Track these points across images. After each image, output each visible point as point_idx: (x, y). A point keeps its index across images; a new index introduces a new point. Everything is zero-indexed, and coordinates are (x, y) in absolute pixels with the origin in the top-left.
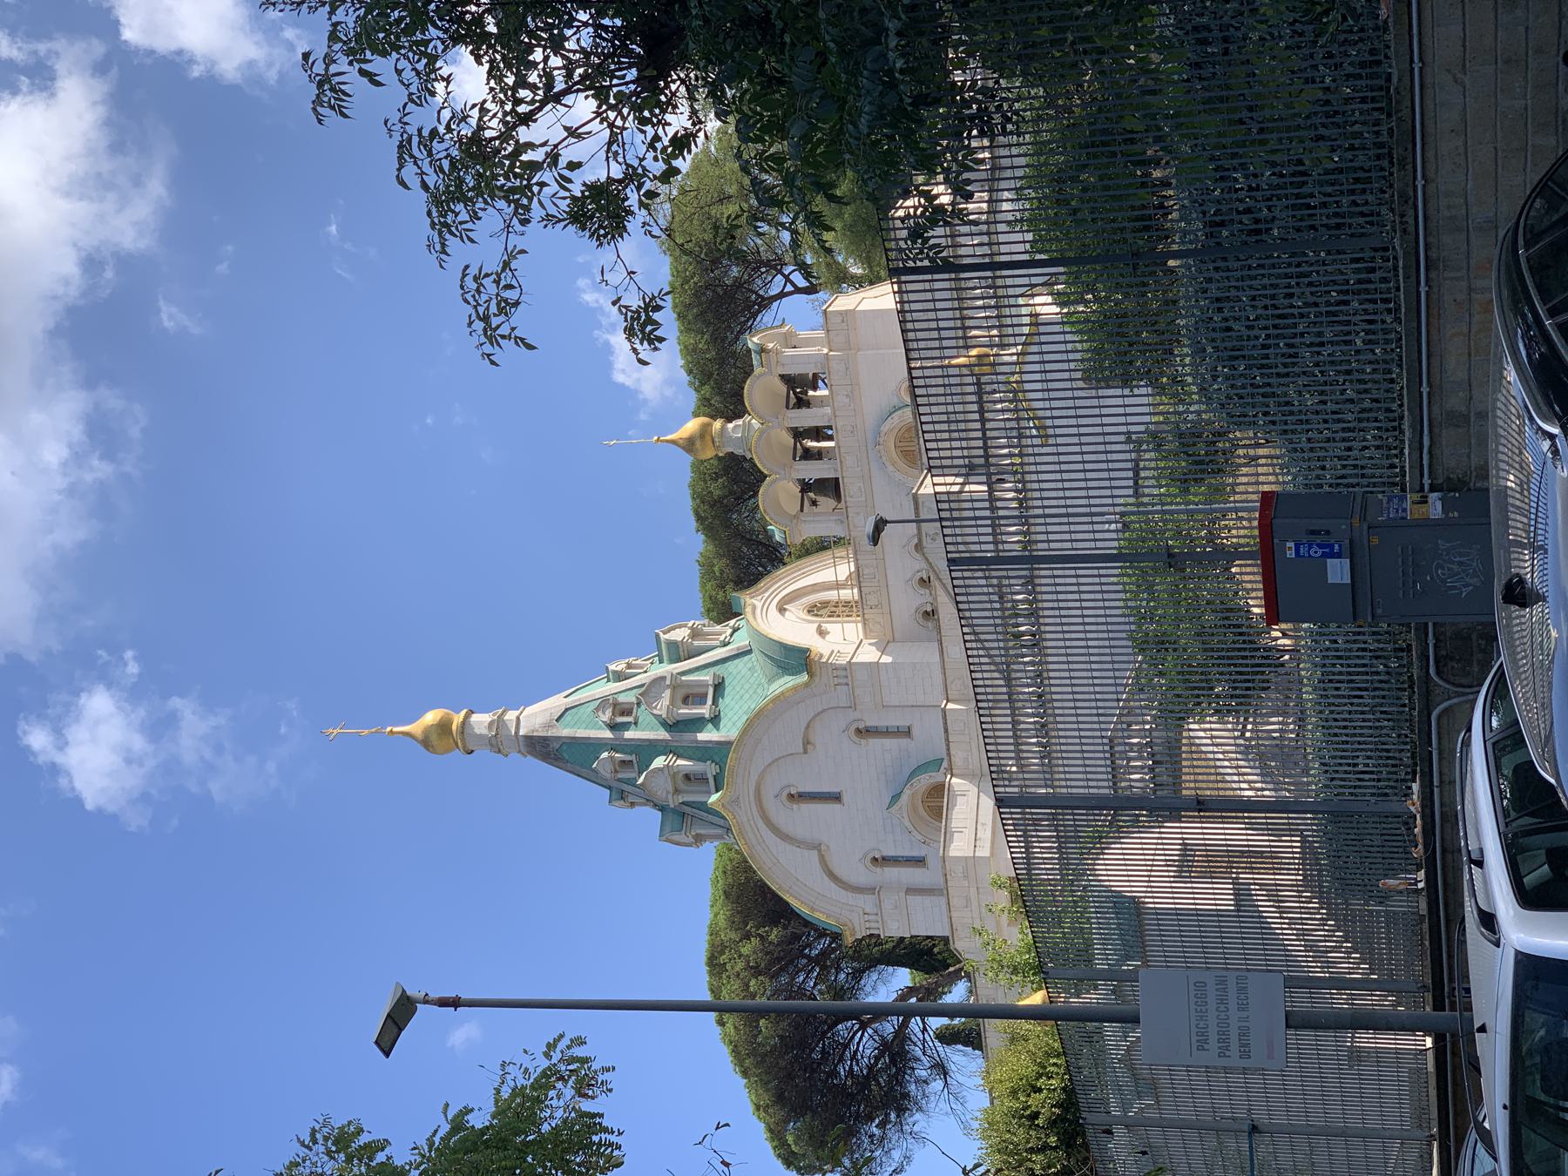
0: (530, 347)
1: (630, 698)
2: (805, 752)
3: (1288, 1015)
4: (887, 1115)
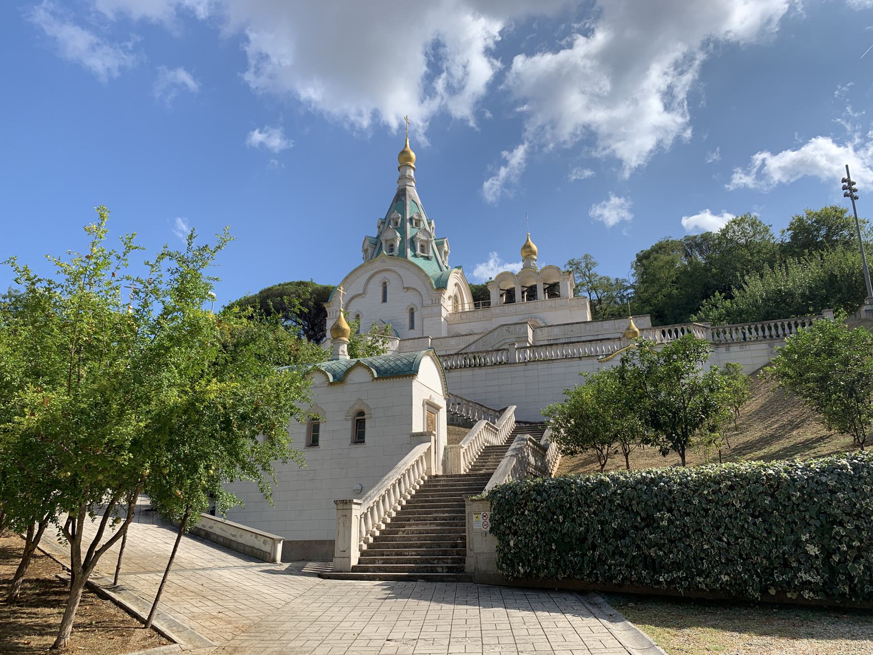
1: (422, 226)
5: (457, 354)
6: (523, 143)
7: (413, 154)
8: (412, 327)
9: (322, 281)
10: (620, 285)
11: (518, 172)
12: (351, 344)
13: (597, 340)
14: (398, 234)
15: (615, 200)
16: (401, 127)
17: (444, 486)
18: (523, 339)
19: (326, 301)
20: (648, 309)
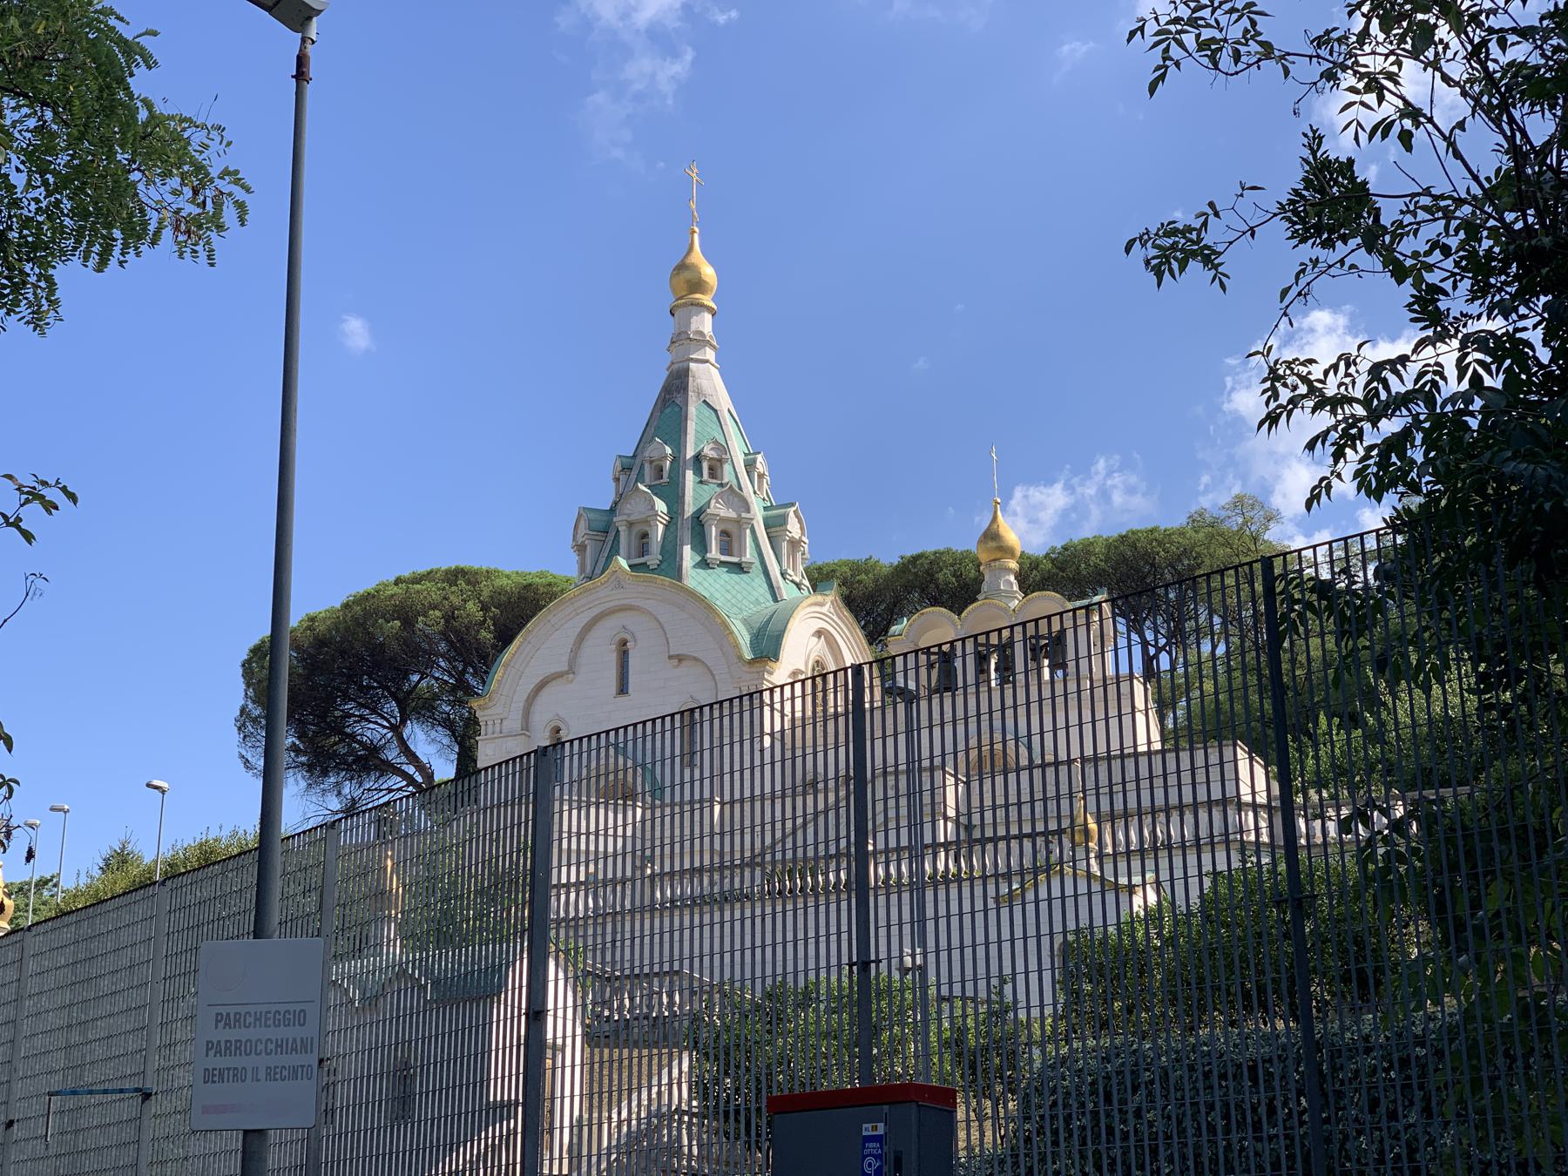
0: (1152, 89)
1: (727, 475)
2: (670, 657)
3: (261, 1133)
4: (305, 753)
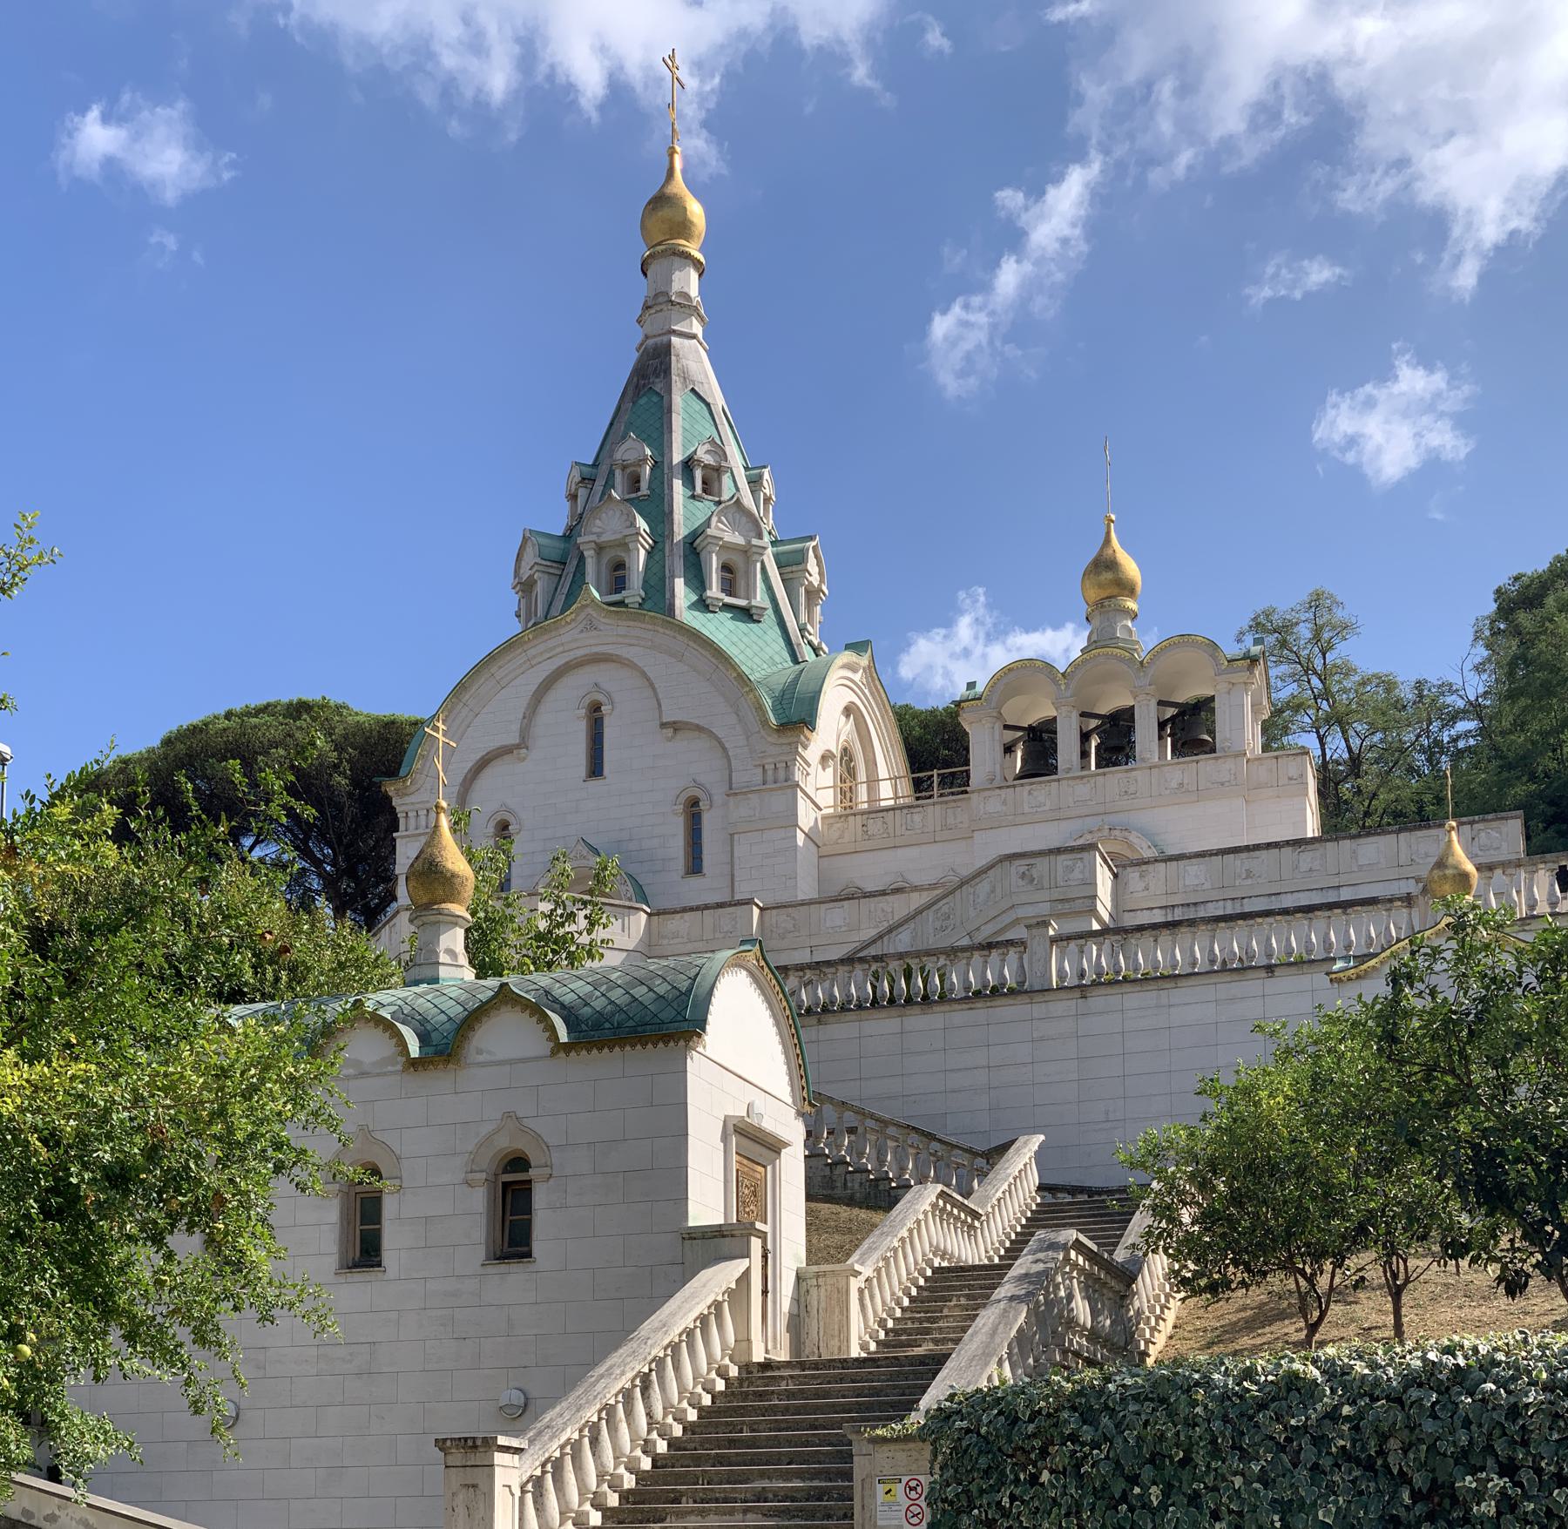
1: (727, 492)
2: (663, 725)
5: (849, 961)
6: (1080, 157)
7: (695, 210)
8: (695, 865)
9: (371, 698)
10: (1429, 704)
11: (1059, 277)
12: (477, 927)
13: (1330, 906)
14: (642, 524)
15: (1412, 381)
16: (618, 90)
17: (790, 1395)
18: (1078, 905)
19: (393, 772)
20: (1520, 790)
